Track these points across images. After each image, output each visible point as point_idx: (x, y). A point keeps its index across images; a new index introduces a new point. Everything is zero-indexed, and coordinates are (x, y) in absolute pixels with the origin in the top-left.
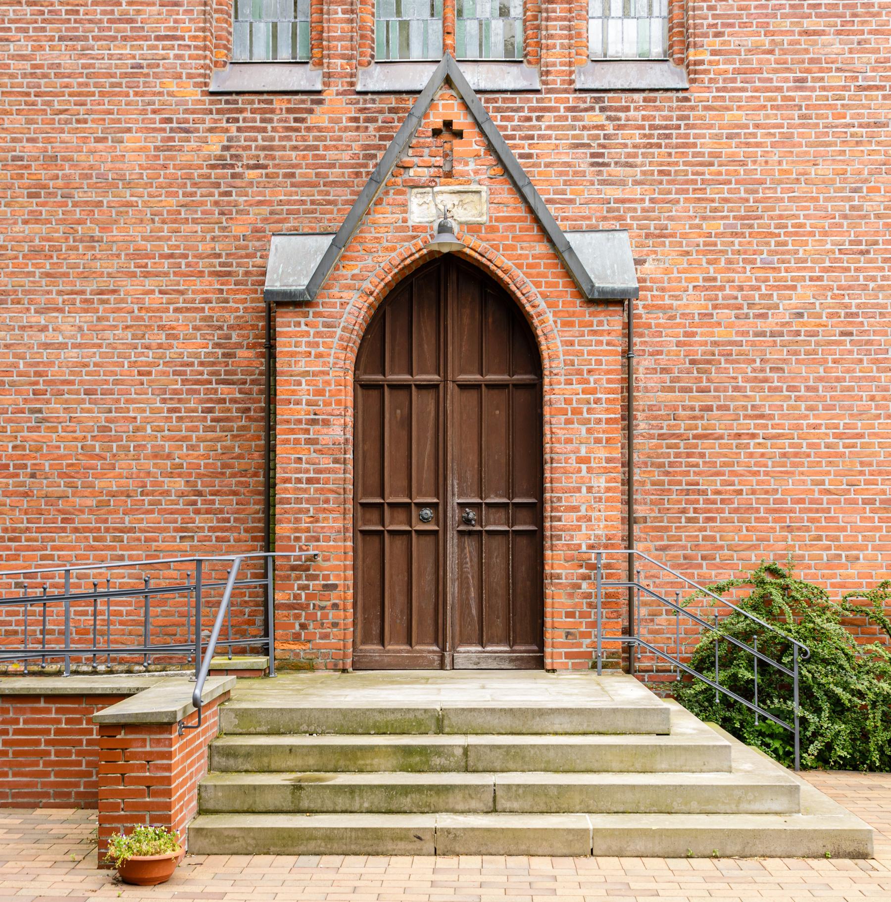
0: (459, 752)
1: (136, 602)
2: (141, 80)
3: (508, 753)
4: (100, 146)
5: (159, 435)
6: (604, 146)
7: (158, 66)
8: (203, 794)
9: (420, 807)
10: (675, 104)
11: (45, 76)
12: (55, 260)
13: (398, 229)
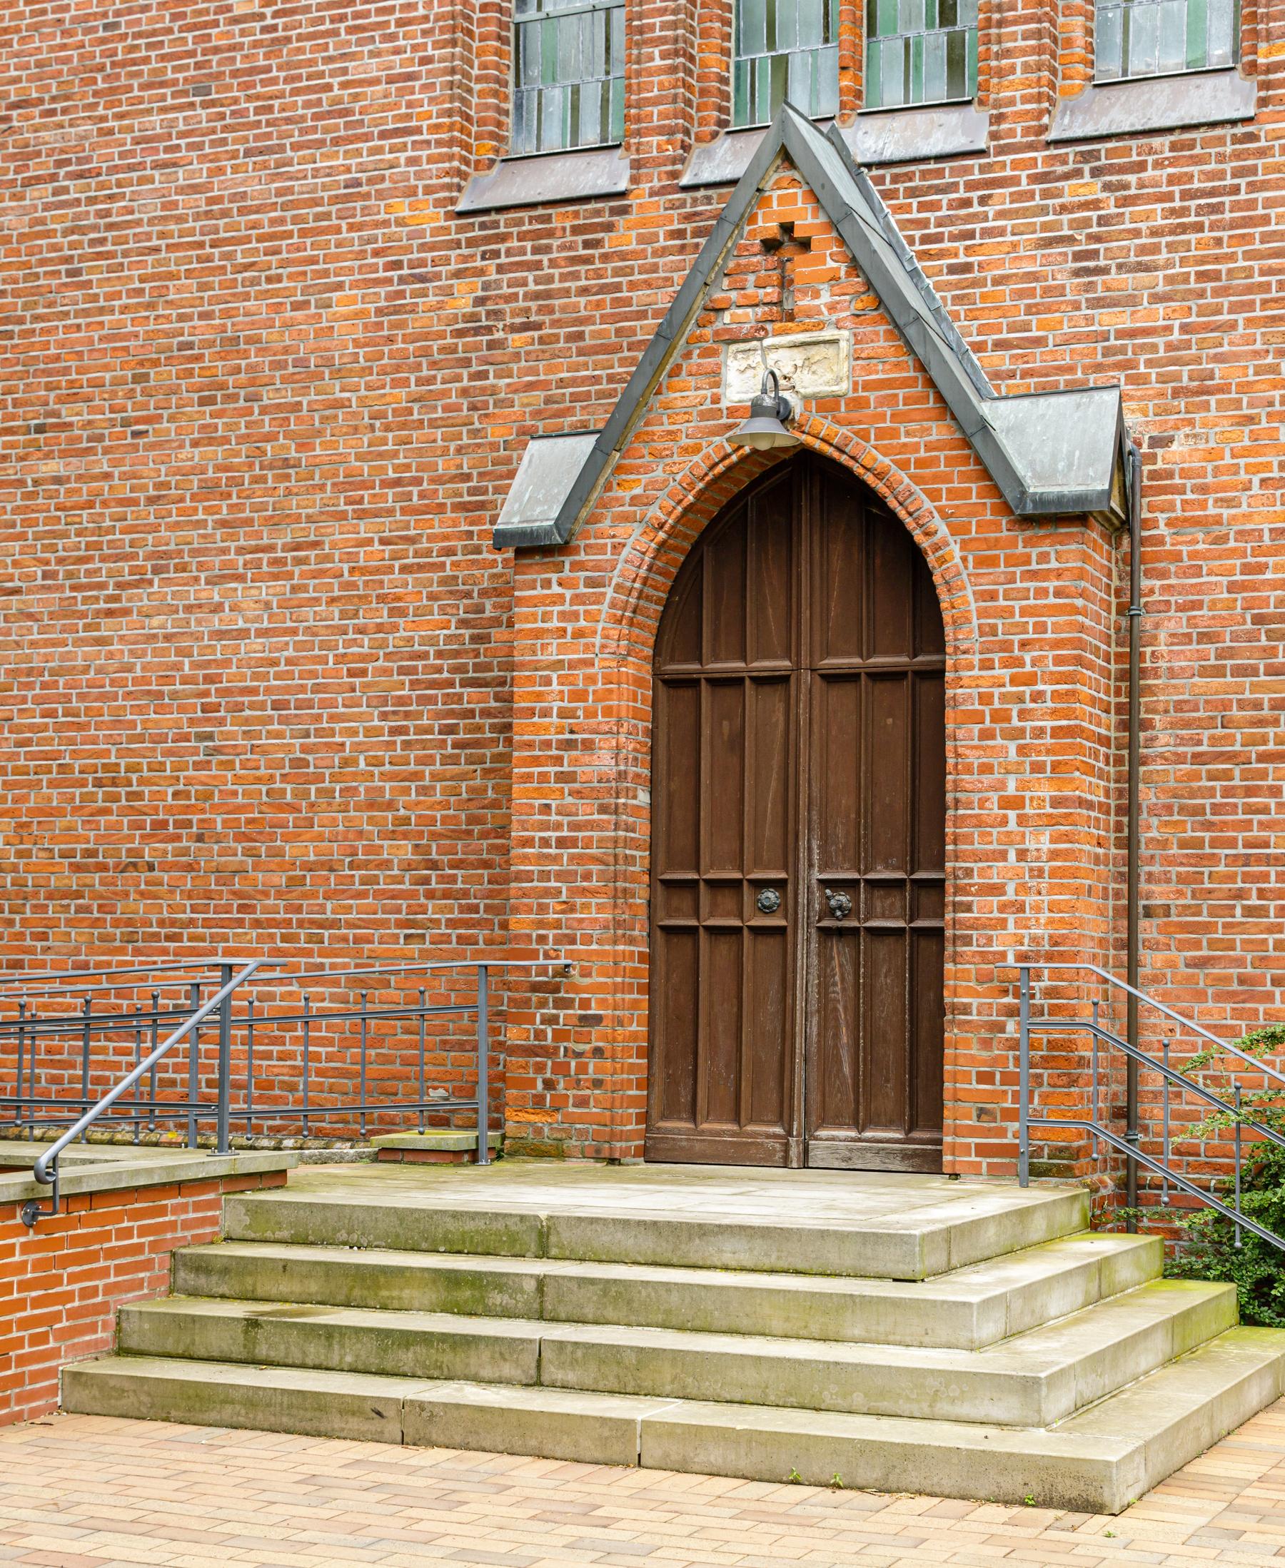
0: (530, 1286)
1: (341, 1040)
2: (359, 205)
3: (605, 1293)
4: (299, 314)
5: (376, 770)
6: (1097, 238)
7: (383, 179)
8: (124, 1325)
9: (427, 1367)
10: (1229, 149)
11: (225, 213)
12: (235, 500)
13: (703, 416)
